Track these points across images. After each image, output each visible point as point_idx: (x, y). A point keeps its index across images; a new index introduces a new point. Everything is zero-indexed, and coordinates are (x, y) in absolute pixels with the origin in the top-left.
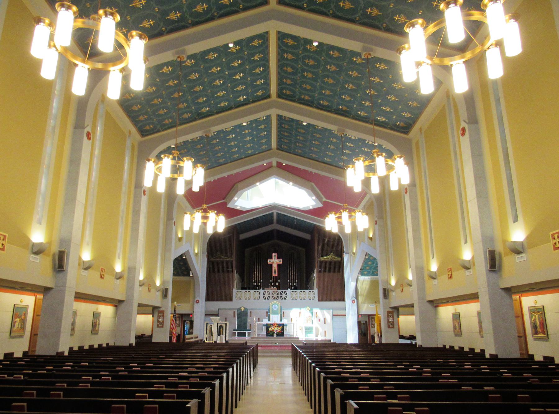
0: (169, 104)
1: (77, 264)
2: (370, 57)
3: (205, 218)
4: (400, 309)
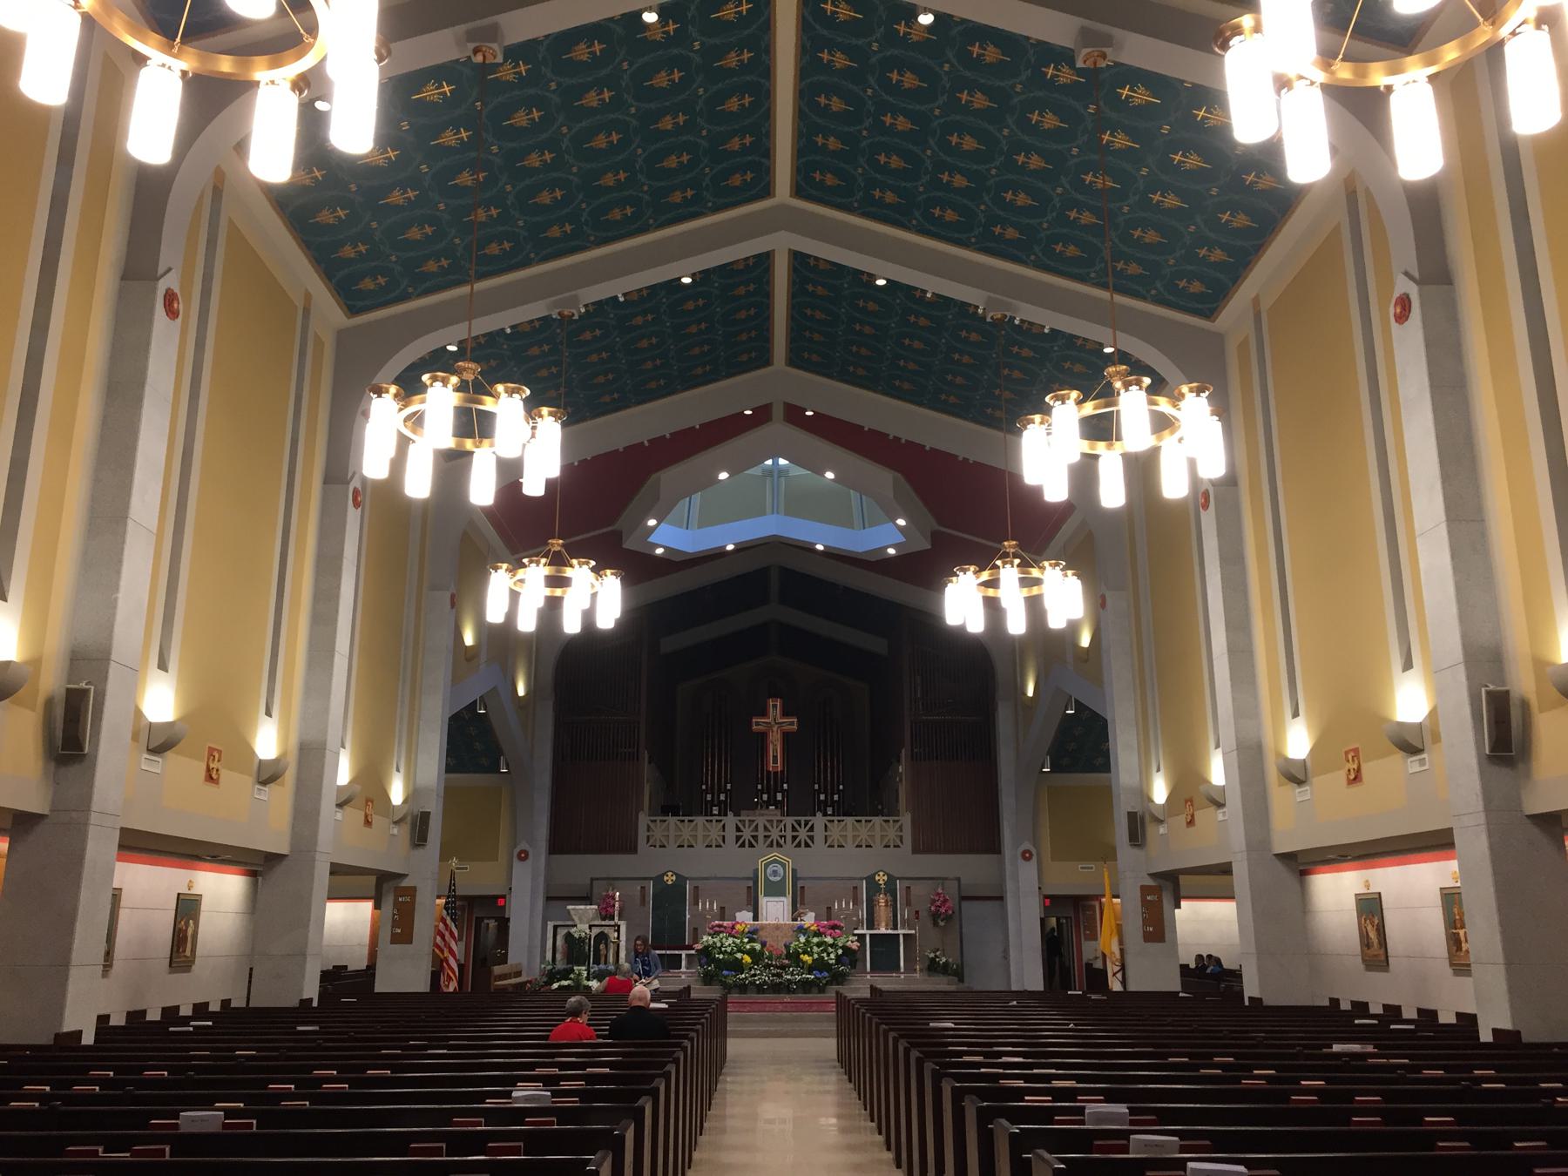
0: (442, 206)
1: (130, 736)
2: (1102, 64)
3: (557, 581)
4: (1183, 879)
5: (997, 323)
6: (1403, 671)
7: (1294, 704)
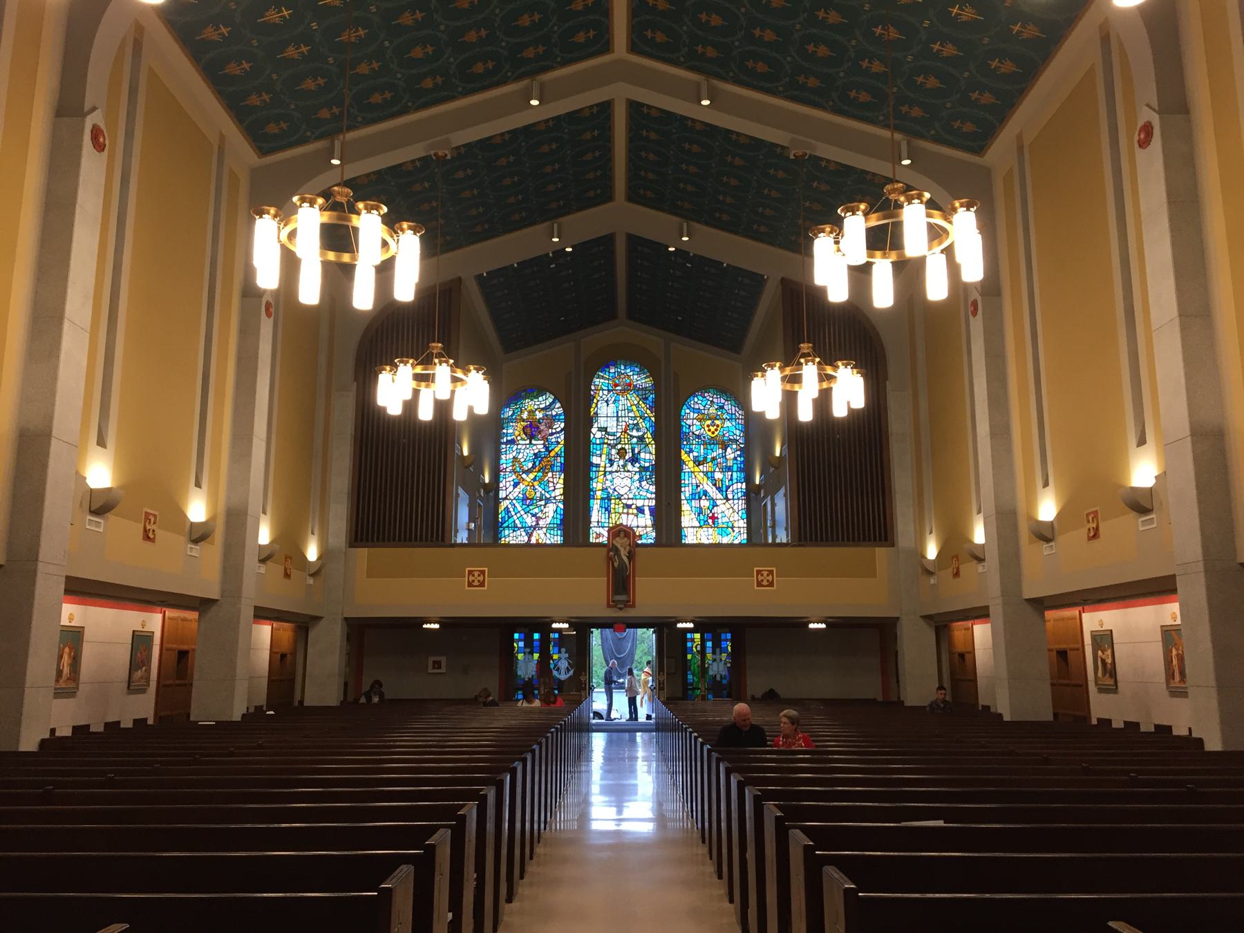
5: (799, 160)
6: (1138, 446)
7: (1045, 477)
